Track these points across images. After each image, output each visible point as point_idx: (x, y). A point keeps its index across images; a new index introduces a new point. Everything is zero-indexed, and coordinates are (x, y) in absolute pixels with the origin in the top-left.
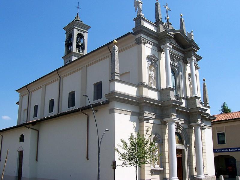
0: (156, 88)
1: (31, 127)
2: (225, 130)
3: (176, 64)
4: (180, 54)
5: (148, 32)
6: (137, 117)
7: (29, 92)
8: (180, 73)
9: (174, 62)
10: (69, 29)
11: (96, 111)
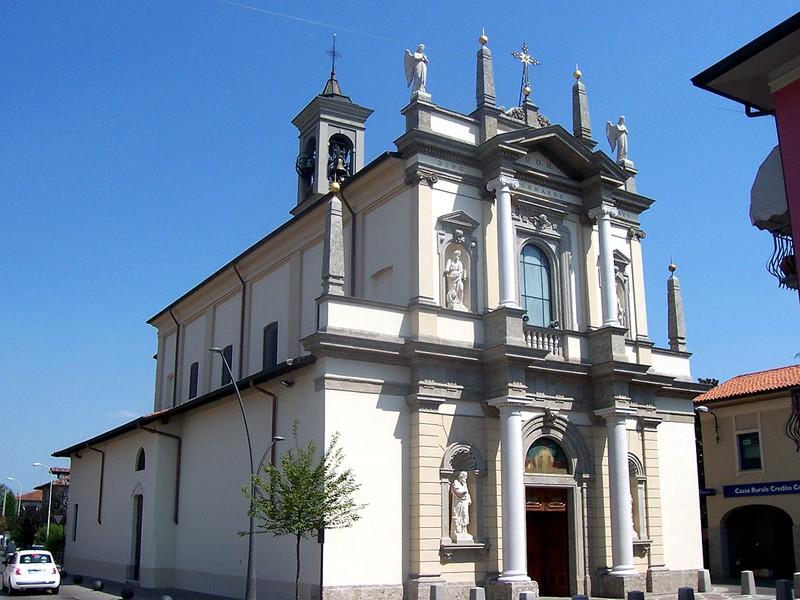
0: (466, 310)
1: (158, 430)
2: (759, 426)
3: (549, 230)
4: (567, 198)
5: (444, 149)
6: (402, 398)
7: (179, 326)
8: (566, 255)
9: (541, 225)
10: (309, 121)
11: (290, 384)
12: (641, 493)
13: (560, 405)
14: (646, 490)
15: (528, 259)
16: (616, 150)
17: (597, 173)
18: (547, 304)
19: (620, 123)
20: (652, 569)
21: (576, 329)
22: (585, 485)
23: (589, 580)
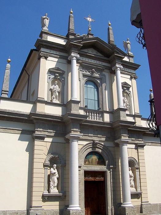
0: (58, 102)
3: (97, 75)
4: (104, 64)
8: (104, 85)
9: (93, 73)
12: (137, 173)
13: (100, 139)
14: (139, 172)
15: (88, 86)
16: (126, 50)
17: (114, 53)
18: (97, 102)
19: (127, 41)
20: (143, 203)
21: (108, 110)
22: (111, 170)
23: (113, 208)
